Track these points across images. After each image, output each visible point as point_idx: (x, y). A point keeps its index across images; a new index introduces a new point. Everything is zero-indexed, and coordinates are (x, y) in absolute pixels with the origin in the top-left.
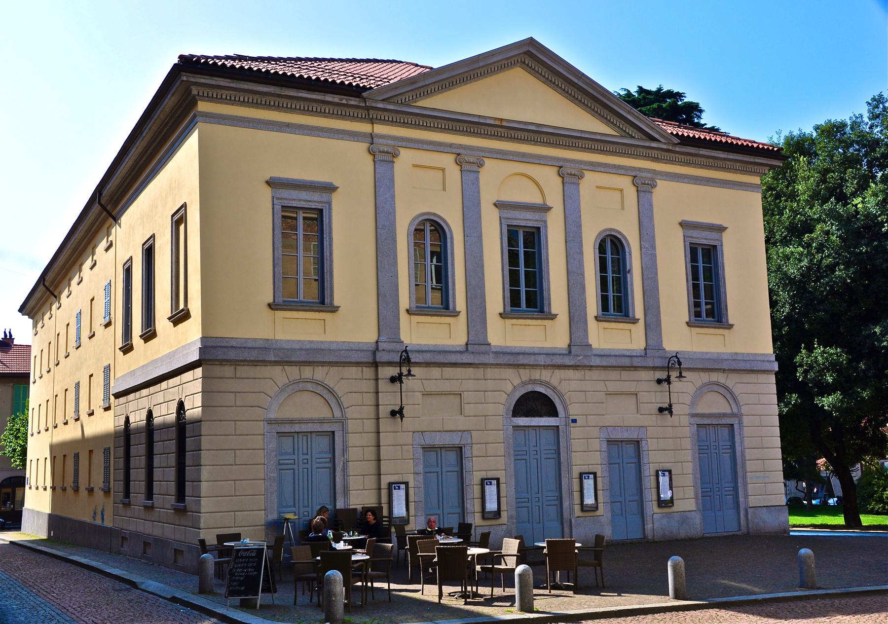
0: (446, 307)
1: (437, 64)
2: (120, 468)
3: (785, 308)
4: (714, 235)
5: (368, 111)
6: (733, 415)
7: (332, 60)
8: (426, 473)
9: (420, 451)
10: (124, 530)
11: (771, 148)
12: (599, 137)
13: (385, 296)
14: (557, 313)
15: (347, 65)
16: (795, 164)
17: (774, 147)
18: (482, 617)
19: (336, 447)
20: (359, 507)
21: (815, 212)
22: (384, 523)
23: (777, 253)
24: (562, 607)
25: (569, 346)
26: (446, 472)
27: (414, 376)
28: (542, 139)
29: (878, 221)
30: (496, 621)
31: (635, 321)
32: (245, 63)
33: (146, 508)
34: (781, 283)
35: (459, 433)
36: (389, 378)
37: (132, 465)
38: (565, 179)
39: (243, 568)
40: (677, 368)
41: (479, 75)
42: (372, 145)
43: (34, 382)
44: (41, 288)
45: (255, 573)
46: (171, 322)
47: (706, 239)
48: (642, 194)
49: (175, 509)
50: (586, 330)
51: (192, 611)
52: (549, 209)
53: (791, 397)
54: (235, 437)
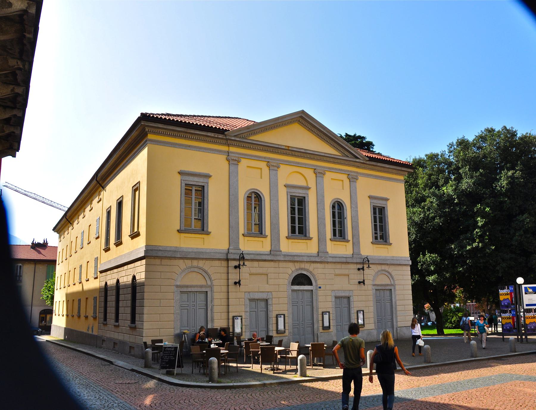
0: (261, 233)
1: (258, 121)
2: (102, 307)
3: (413, 236)
4: (384, 202)
5: (227, 141)
6: (391, 285)
7: (210, 117)
8: (250, 311)
9: (248, 301)
10: (104, 336)
11: (408, 164)
12: (333, 156)
13: (233, 227)
14: (312, 237)
15: (216, 119)
16: (417, 171)
17: (410, 163)
18: (283, 379)
19: (208, 299)
20: (219, 328)
21: (426, 193)
22: (231, 335)
23: (410, 211)
24: (320, 374)
25: (318, 252)
26: (260, 311)
27: (246, 265)
28: (307, 156)
29: (453, 197)
30: (290, 381)
31: (348, 241)
32: (171, 117)
33: (115, 326)
34: (411, 224)
35: (267, 293)
36: (234, 266)
37: (108, 305)
38: (317, 175)
39: (168, 356)
40: (367, 263)
41: (279, 126)
42: (228, 156)
43: (59, 264)
44: (65, 219)
45: (174, 358)
46: (130, 237)
47: (380, 204)
48: (351, 182)
49: (130, 327)
50: (326, 245)
51: (143, 376)
52: (309, 188)
53: (415, 277)
54: (160, 293)
